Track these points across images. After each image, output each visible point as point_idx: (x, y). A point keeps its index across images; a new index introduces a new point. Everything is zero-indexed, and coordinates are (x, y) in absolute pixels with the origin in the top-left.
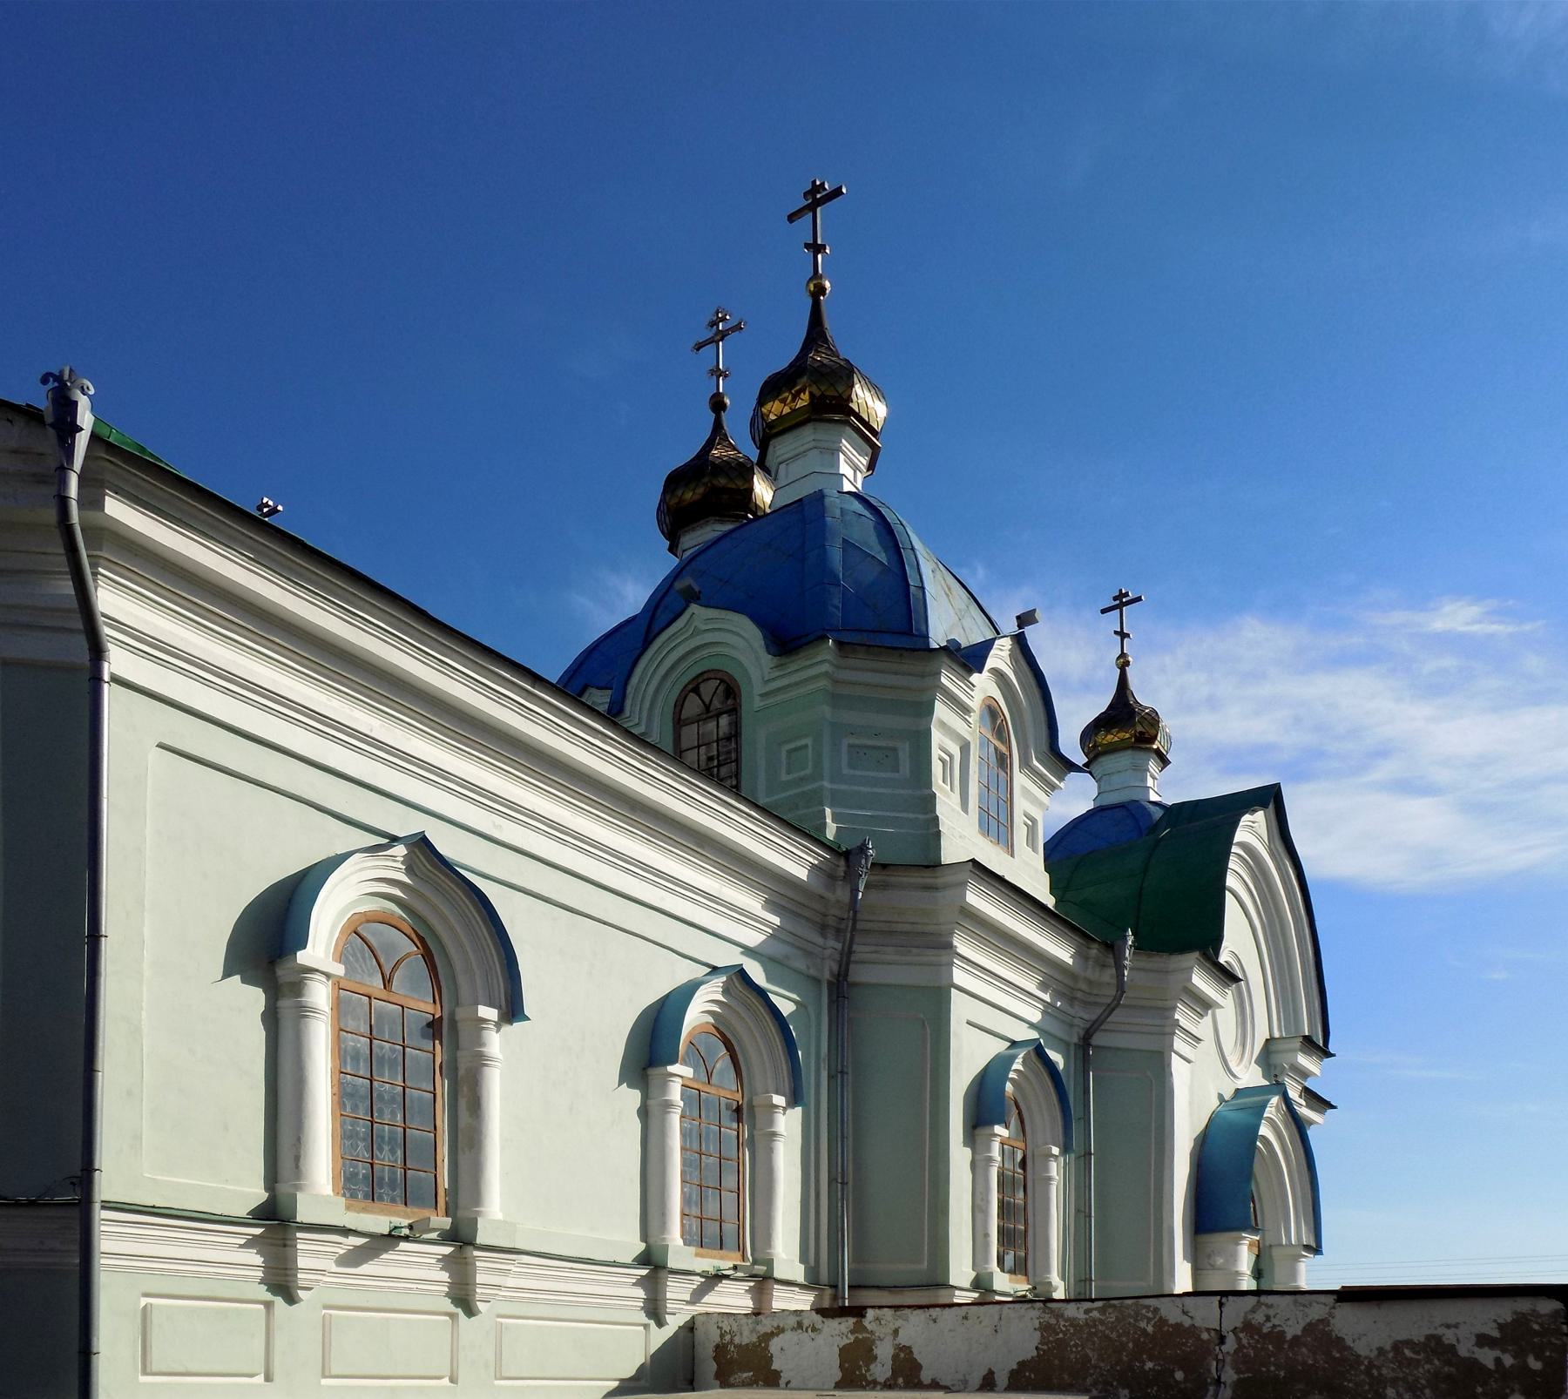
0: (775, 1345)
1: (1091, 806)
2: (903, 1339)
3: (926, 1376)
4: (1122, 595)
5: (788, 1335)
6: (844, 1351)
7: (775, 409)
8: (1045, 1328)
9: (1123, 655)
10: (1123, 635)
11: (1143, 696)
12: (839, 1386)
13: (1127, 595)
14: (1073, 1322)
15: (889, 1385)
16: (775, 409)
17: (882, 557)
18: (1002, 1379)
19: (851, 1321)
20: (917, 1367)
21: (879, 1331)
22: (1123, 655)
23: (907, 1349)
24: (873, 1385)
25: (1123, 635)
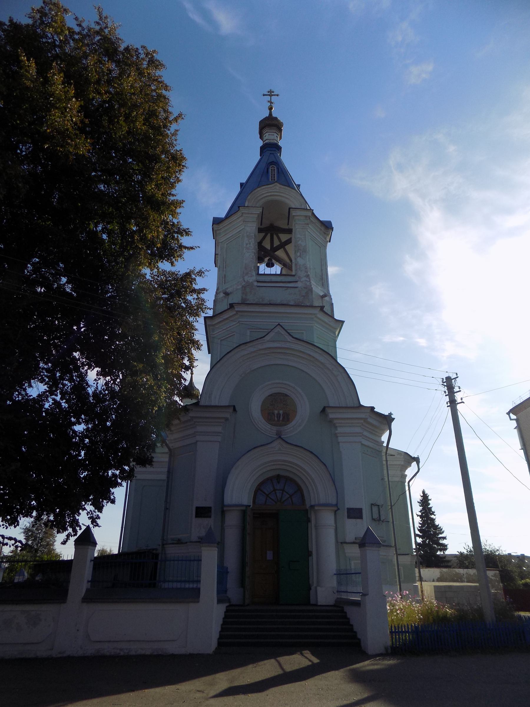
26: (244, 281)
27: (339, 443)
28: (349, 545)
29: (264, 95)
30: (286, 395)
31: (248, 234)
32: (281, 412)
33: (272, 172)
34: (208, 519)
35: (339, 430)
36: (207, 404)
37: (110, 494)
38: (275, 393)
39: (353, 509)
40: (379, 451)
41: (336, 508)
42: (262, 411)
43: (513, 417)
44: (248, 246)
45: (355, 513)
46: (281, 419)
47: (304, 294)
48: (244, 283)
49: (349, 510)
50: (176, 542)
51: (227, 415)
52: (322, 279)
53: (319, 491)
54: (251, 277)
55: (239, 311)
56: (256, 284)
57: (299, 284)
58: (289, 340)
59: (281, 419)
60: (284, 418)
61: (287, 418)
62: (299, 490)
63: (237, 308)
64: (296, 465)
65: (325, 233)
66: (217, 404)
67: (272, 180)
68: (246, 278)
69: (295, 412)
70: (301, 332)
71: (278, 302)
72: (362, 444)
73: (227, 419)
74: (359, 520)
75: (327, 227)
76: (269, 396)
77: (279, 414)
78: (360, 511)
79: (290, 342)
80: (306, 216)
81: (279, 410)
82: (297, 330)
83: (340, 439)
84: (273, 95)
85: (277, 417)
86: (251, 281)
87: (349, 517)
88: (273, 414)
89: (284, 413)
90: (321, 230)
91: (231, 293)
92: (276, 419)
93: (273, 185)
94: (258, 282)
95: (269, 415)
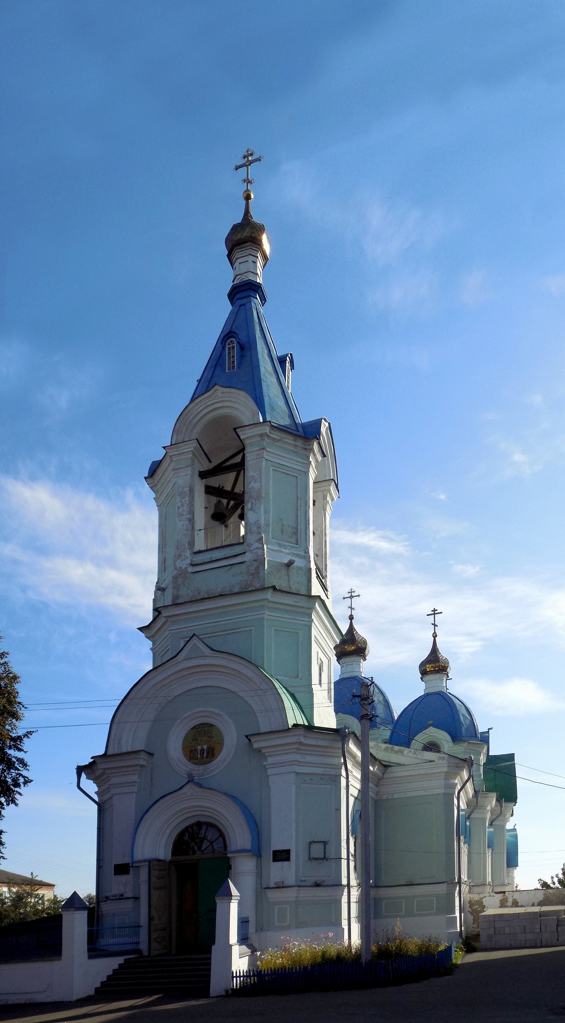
0: (484, 900)
1: (422, 693)
2: (514, 897)
3: (520, 904)
4: (434, 610)
5: (487, 898)
6: (501, 901)
7: (238, 459)
8: (545, 894)
9: (435, 633)
10: (435, 625)
11: (443, 652)
12: (500, 907)
13: (437, 610)
14: (550, 893)
15: (511, 907)
16: (238, 459)
17: (469, 718)
18: (536, 904)
19: (502, 894)
20: (517, 903)
21: (509, 896)
22: (435, 633)
23: (515, 899)
24: (508, 907)
25: (435, 625)
26: (176, 569)
27: (268, 776)
28: (273, 890)
29: (237, 168)
30: (211, 725)
31: (180, 490)
32: (205, 747)
33: (229, 353)
34: (126, 876)
35: (270, 760)
36: (116, 751)
37: (504, 831)
38: (200, 725)
39: (279, 851)
40: (337, 776)
41: (256, 851)
42: (183, 749)
43: (91, 787)
44: (181, 510)
45: (282, 856)
46: (205, 755)
47: (253, 571)
48: (176, 572)
49: (275, 852)
50: (118, 897)
51: (142, 762)
52: (296, 532)
53: (239, 836)
54: (184, 560)
55: (170, 616)
56: (191, 569)
57: (248, 557)
58: (207, 654)
59: (205, 755)
60: (208, 753)
61: (211, 754)
62: (222, 835)
63: (165, 613)
64: (209, 808)
65: (305, 449)
66: (130, 749)
67: (229, 369)
68: (179, 564)
69: (221, 744)
70: (249, 629)
71: (218, 591)
72: (296, 773)
73: (142, 766)
74: (285, 863)
75: (308, 433)
76: (192, 729)
77: (202, 750)
78: (288, 852)
79: (207, 656)
80: (261, 435)
81: (203, 744)
82: (246, 627)
83: (269, 772)
84: (251, 162)
85: (201, 754)
86: (184, 567)
87: (275, 860)
88: (196, 750)
89: (208, 748)
90: (296, 446)
91: (166, 588)
92: (199, 756)
93: (212, 391)
94: (193, 565)
95: (192, 754)
